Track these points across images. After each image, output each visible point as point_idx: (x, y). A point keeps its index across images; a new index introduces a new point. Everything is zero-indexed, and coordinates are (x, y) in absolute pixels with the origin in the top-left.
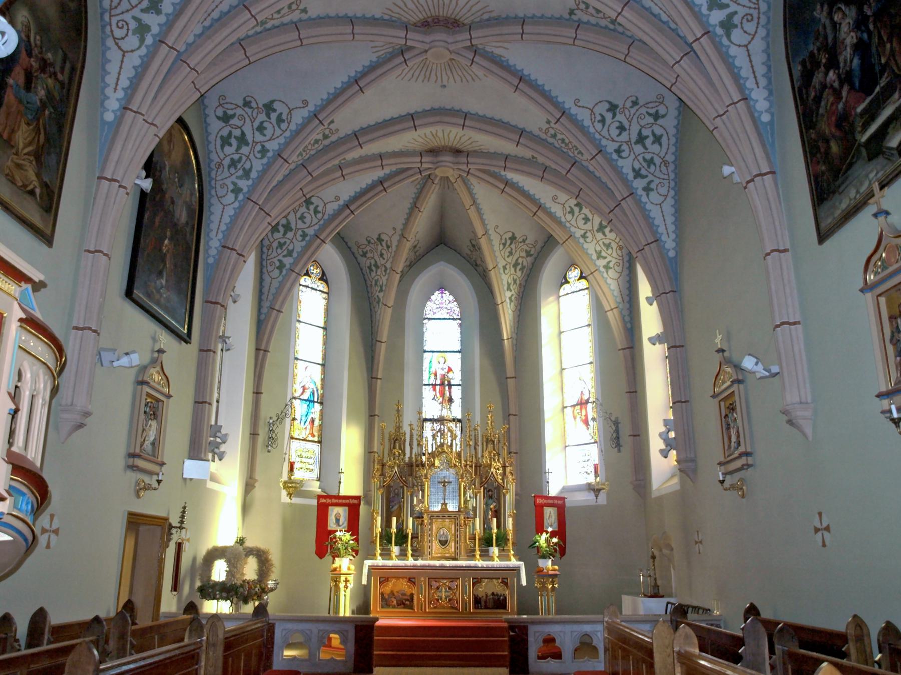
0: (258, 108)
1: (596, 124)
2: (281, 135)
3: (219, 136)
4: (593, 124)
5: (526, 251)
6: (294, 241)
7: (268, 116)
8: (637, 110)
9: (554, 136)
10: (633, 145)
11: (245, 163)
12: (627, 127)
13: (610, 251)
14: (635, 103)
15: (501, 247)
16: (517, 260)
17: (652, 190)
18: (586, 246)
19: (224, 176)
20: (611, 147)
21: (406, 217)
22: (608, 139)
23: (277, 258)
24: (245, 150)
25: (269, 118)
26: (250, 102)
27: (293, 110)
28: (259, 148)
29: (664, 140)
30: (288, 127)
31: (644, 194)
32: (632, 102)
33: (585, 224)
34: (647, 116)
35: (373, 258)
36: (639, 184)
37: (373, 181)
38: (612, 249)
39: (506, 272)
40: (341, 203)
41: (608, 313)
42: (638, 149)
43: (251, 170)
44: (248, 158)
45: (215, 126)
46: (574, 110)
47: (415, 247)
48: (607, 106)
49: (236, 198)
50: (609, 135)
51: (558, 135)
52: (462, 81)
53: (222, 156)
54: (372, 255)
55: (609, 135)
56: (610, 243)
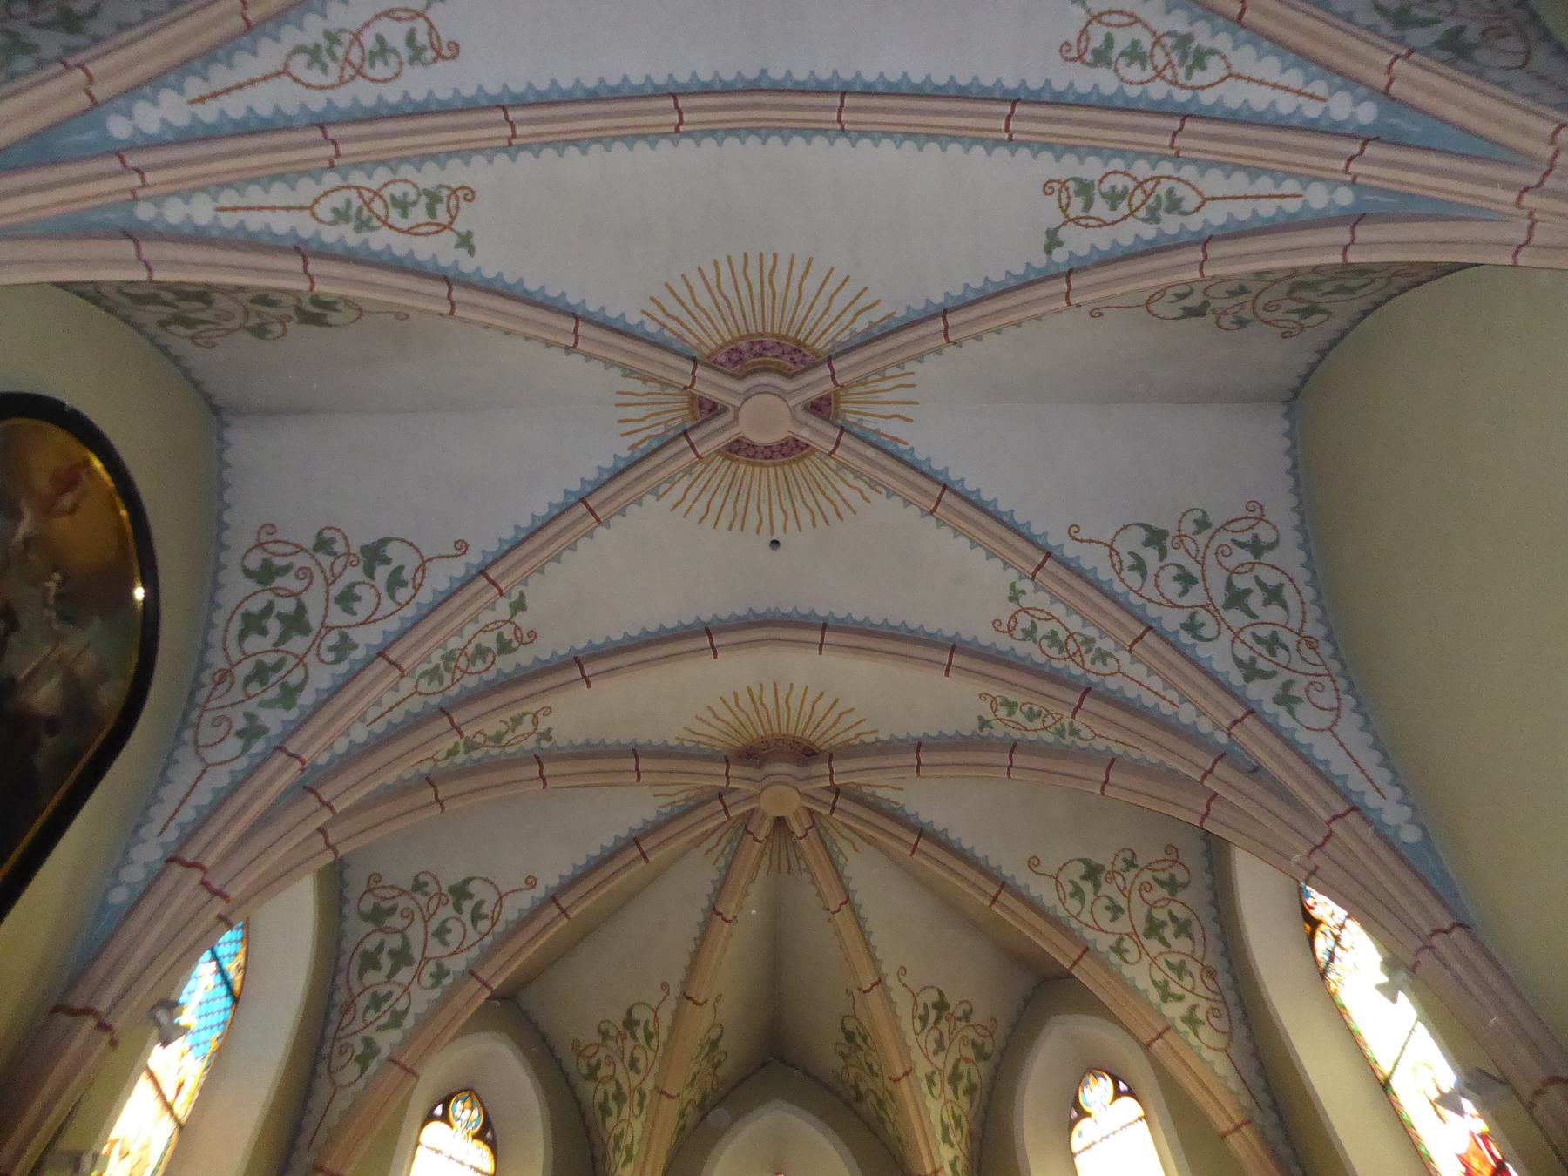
0: (348, 554)
1: (1125, 574)
2: (393, 613)
3: (241, 610)
4: (1119, 575)
5: (974, 1045)
6: (311, 659)
7: (370, 572)
8: (1211, 538)
9: (1030, 634)
10: (1222, 611)
11: (289, 672)
12: (1197, 574)
13: (1187, 982)
14: (1202, 524)
15: (918, 1022)
16: (956, 1066)
17: (1298, 700)
18: (1127, 971)
19: (227, 700)
20: (1172, 621)
21: (692, 947)
22: (1160, 604)
23: (360, 1035)
24: (298, 644)
25: (372, 577)
26: (332, 541)
27: (430, 559)
28: (333, 638)
29: (1289, 593)
30: (413, 597)
31: (1282, 711)
32: (1196, 521)
33: (1114, 919)
34: (1236, 549)
35: (612, 1077)
36: (1260, 691)
37: (617, 838)
38: (1191, 976)
39: (936, 1091)
40: (540, 892)
41: (1231, 1138)
42: (1235, 618)
43: (301, 686)
44: (301, 660)
45: (238, 590)
46: (1071, 550)
47: (714, 1044)
48: (1142, 534)
49: (245, 749)
50: (1162, 594)
51: (1039, 624)
52: (814, 525)
53: (235, 655)
54: (609, 1071)
55: (1162, 594)
56: (1183, 963)
